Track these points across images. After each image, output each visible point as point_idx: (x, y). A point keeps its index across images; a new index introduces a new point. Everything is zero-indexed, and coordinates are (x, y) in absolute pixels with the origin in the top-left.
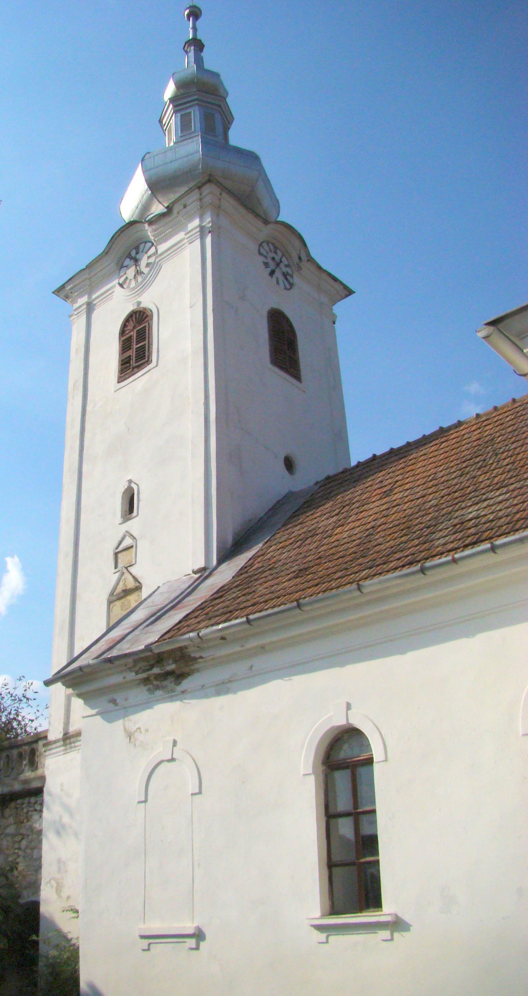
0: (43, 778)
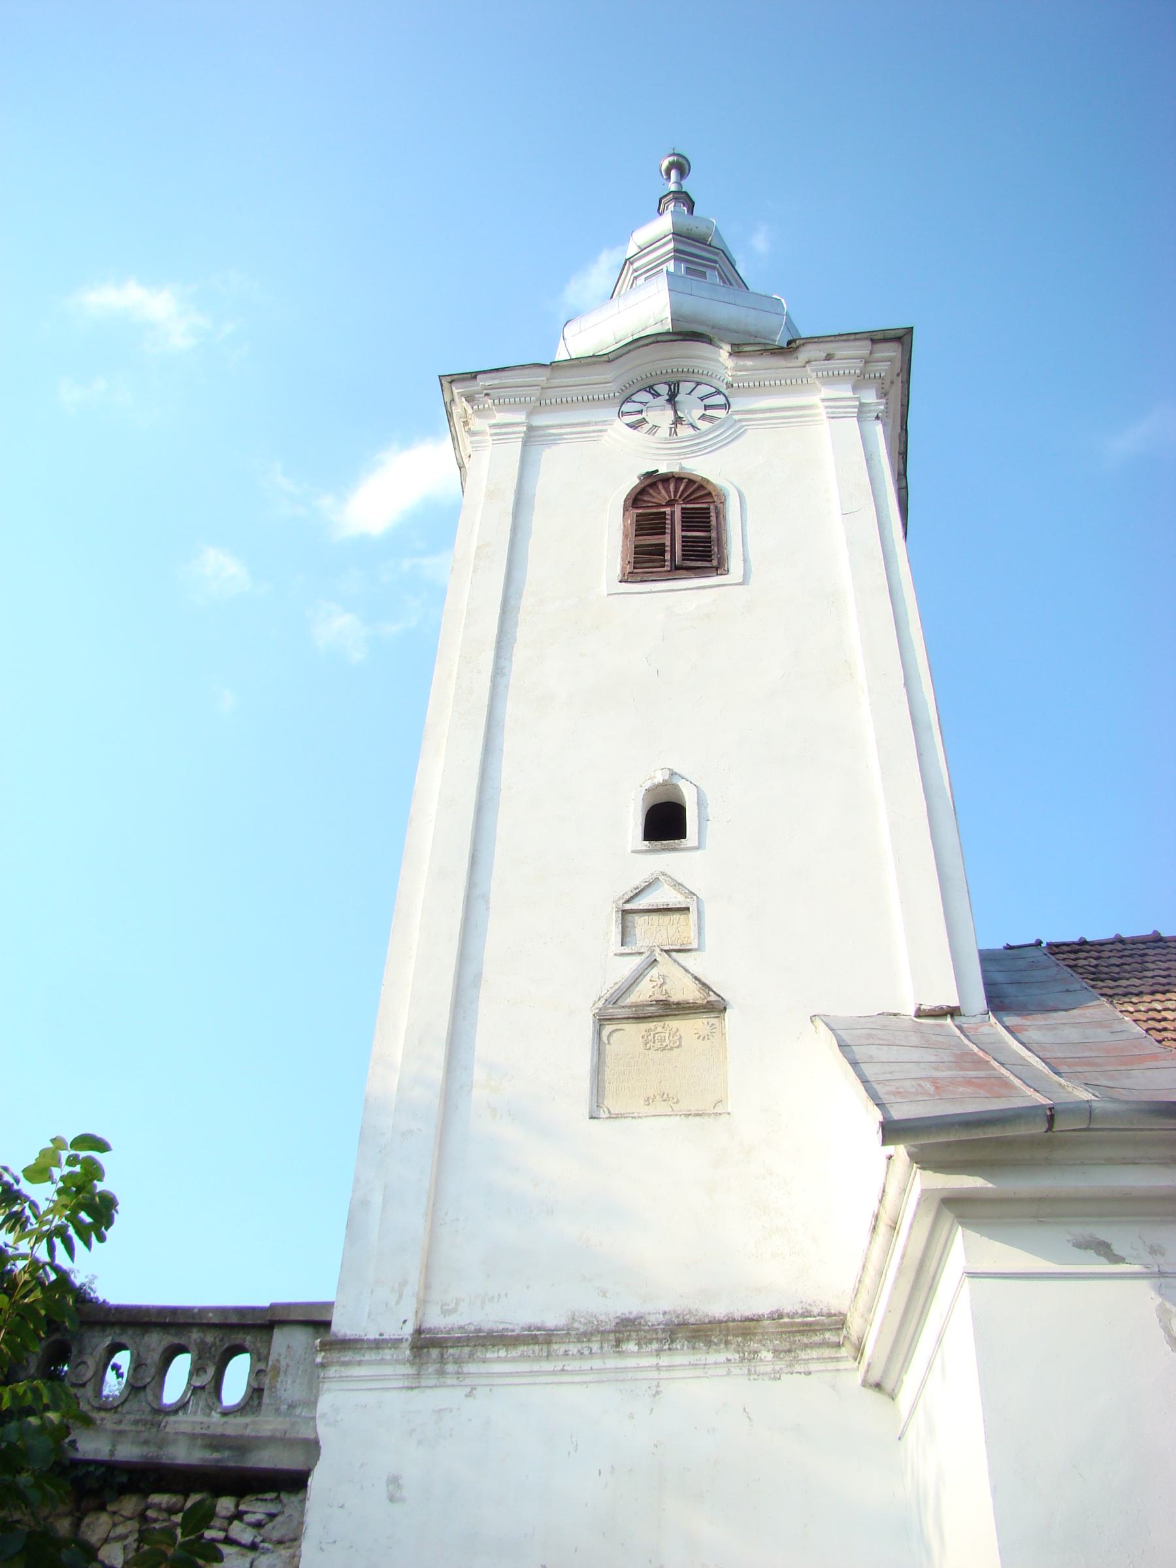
0: (313, 1447)
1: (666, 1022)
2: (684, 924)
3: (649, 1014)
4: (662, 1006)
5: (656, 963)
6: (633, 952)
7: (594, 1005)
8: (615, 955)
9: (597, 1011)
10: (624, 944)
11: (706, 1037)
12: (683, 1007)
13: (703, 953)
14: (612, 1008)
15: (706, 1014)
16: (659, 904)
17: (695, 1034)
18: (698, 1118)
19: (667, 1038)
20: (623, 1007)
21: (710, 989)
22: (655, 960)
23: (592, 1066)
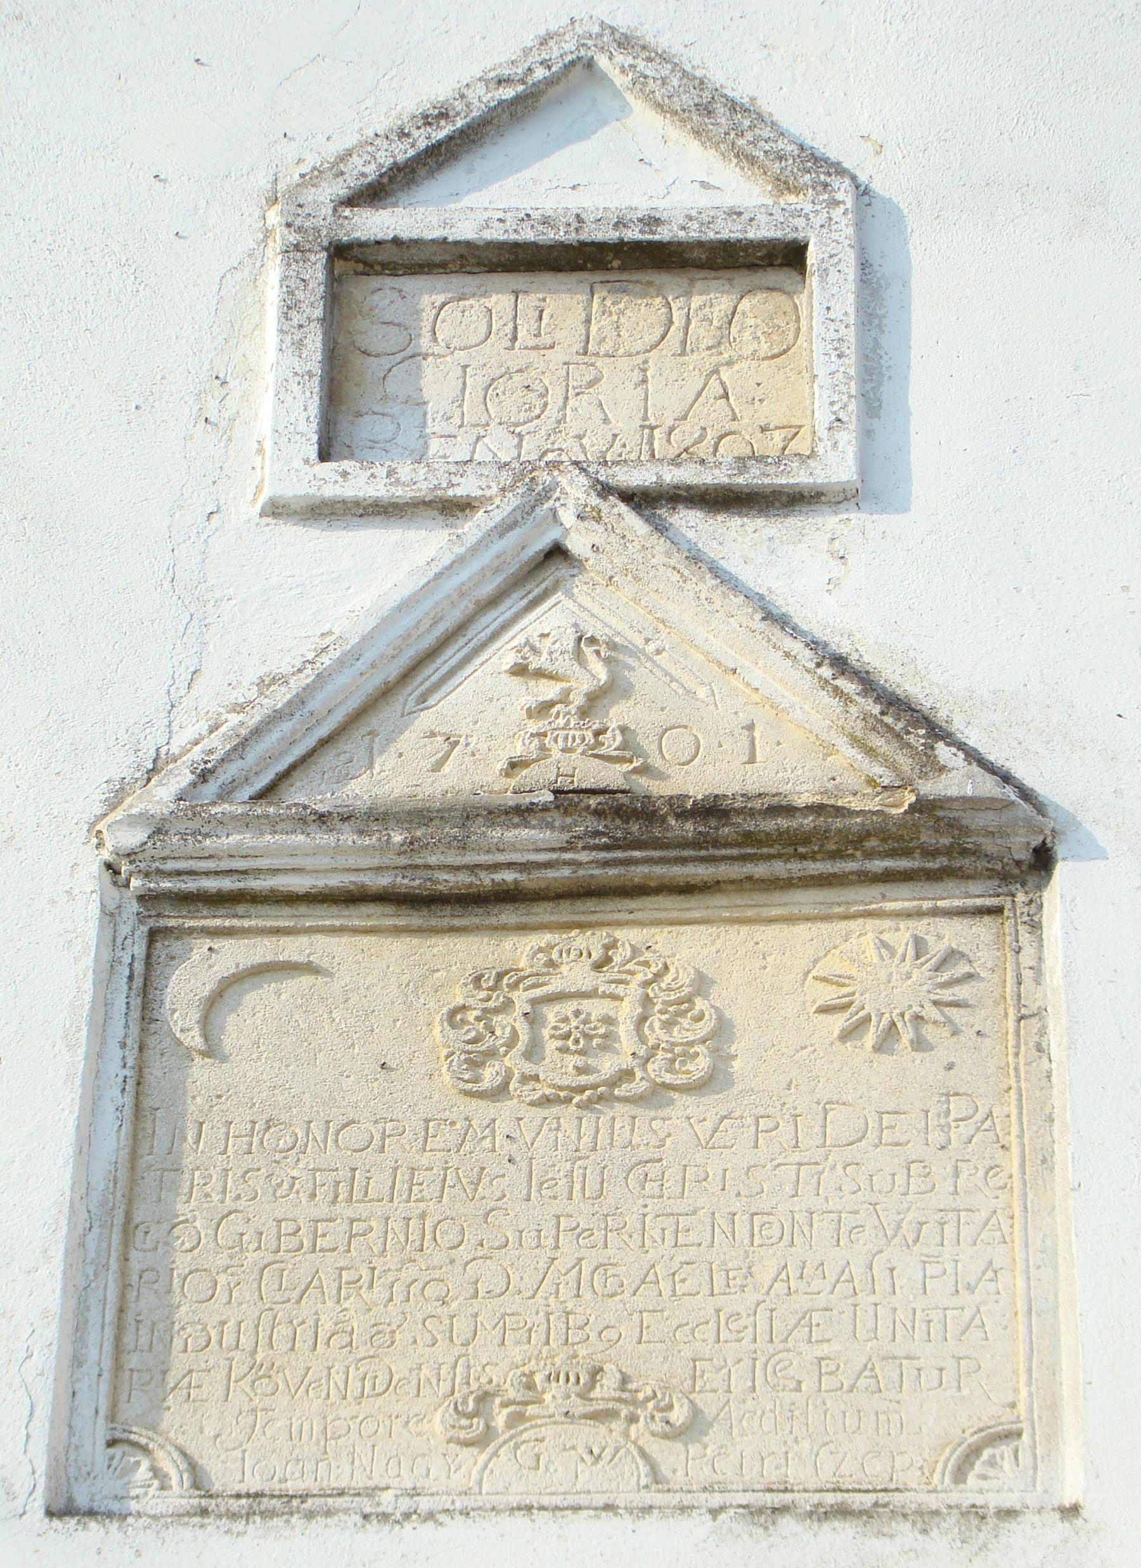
1: (628, 936)
2: (764, 348)
3: (509, 876)
4: (593, 824)
5: (557, 570)
6: (401, 493)
7: (113, 805)
8: (276, 510)
9: (134, 838)
10: (337, 447)
11: (907, 1034)
12: (749, 838)
13: (886, 521)
14: (245, 822)
15: (904, 890)
16: (589, 217)
17: (825, 1010)
18: (842, 1533)
19: (625, 1030)
20: (322, 818)
21: (937, 732)
22: (557, 552)
23: (83, 1186)
